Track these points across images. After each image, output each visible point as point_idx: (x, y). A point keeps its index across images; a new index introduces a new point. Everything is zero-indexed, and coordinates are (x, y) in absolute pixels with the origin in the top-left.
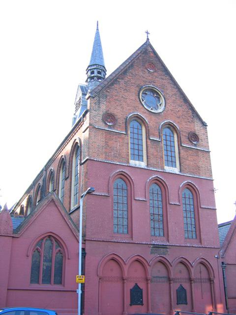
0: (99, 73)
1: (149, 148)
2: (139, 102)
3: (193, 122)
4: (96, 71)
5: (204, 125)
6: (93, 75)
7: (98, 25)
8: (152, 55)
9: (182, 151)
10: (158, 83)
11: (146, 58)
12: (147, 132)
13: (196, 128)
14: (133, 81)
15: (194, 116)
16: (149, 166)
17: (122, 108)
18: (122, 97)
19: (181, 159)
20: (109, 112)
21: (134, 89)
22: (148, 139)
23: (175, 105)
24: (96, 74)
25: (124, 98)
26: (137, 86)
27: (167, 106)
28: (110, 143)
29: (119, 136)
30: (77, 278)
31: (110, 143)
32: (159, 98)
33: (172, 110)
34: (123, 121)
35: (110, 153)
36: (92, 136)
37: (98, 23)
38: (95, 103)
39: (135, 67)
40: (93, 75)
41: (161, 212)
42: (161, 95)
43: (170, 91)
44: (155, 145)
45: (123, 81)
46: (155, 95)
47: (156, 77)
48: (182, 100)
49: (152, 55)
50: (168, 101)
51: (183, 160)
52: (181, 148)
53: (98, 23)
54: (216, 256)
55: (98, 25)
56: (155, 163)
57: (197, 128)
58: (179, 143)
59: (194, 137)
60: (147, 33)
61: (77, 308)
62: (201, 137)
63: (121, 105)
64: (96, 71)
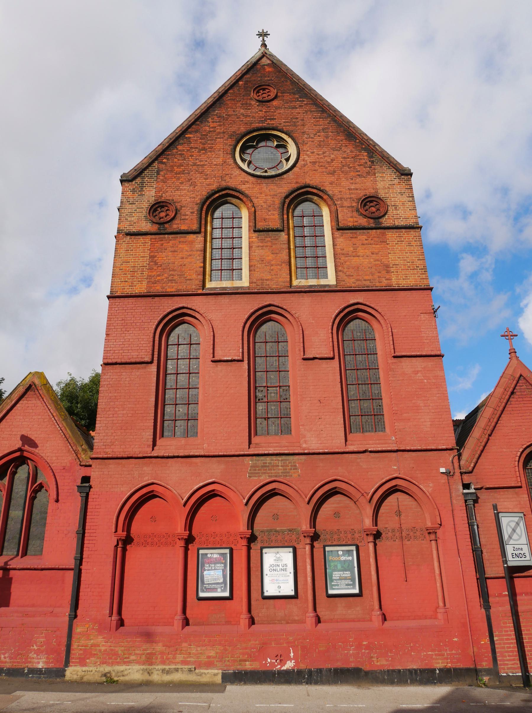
11: (264, 98)
13: (380, 185)
15: (373, 162)
16: (368, 336)
18: (195, 164)
23: (325, 149)
26: (231, 136)
29: (182, 239)
31: (164, 257)
32: (285, 147)
33: (314, 163)
35: (159, 276)
36: (122, 251)
38: (133, 191)
39: (228, 102)
41: (261, 407)
45: (198, 135)
46: (276, 143)
48: (341, 137)
52: (72, 672)
54: (443, 470)
56: (269, 277)
57: (383, 183)
59: (372, 207)
61: (335, 256)
63: (189, 180)
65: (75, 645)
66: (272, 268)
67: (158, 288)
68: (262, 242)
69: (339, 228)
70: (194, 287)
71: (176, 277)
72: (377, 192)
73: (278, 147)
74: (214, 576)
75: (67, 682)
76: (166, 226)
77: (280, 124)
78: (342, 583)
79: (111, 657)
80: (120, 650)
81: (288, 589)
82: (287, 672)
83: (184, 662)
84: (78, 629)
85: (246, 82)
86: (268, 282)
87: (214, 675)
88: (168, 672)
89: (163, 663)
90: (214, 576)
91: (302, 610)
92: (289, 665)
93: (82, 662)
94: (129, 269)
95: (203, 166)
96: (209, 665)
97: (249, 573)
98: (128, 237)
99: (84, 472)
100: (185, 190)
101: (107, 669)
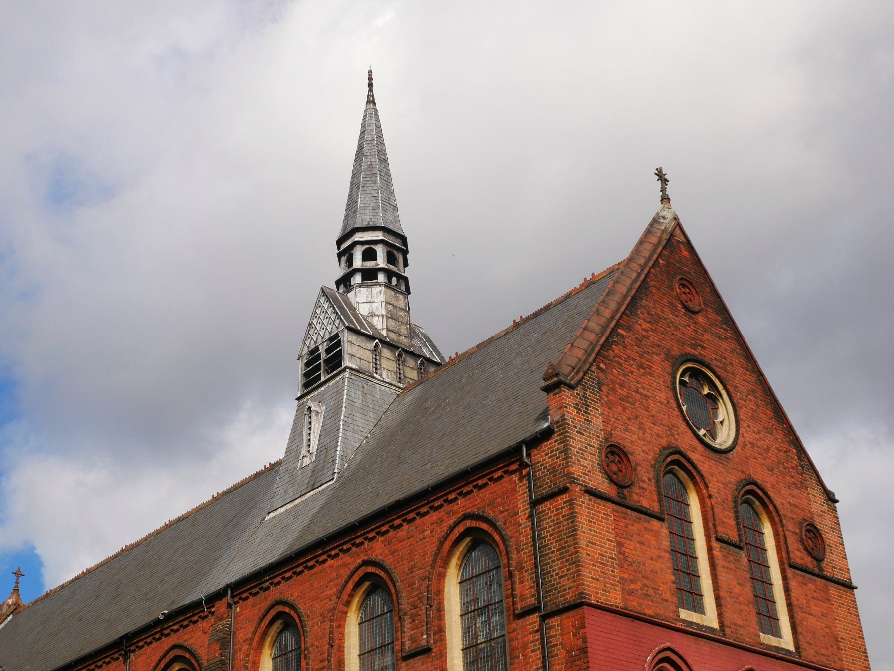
0: (391, 259)
1: (719, 569)
2: (677, 412)
3: (803, 486)
4: (381, 250)
5: (831, 499)
6: (370, 264)
7: (370, 86)
9: (793, 584)
10: (714, 348)
12: (710, 516)
14: (654, 338)
15: (802, 467)
18: (637, 391)
19: (795, 609)
20: (614, 440)
21: (659, 366)
22: (716, 545)
25: (641, 394)
27: (742, 430)
28: (631, 546)
29: (646, 524)
33: (753, 444)
34: (648, 473)
35: (632, 582)
37: (370, 79)
40: (370, 264)
42: (724, 393)
43: (741, 380)
44: (731, 558)
46: (706, 391)
47: (705, 330)
49: (686, 253)
50: (741, 414)
51: (799, 616)
52: (790, 572)
53: (370, 79)
55: (370, 86)
58: (784, 555)
64: (381, 250)
66: (742, 607)
67: (634, 605)
68: (726, 561)
69: (786, 564)
70: (672, 615)
71: (651, 592)
72: (812, 518)
73: (708, 395)
76: (625, 491)
77: (712, 360)
85: (668, 264)
86: (741, 631)
94: (597, 558)
95: (647, 397)
98: (587, 497)
100: (634, 433)
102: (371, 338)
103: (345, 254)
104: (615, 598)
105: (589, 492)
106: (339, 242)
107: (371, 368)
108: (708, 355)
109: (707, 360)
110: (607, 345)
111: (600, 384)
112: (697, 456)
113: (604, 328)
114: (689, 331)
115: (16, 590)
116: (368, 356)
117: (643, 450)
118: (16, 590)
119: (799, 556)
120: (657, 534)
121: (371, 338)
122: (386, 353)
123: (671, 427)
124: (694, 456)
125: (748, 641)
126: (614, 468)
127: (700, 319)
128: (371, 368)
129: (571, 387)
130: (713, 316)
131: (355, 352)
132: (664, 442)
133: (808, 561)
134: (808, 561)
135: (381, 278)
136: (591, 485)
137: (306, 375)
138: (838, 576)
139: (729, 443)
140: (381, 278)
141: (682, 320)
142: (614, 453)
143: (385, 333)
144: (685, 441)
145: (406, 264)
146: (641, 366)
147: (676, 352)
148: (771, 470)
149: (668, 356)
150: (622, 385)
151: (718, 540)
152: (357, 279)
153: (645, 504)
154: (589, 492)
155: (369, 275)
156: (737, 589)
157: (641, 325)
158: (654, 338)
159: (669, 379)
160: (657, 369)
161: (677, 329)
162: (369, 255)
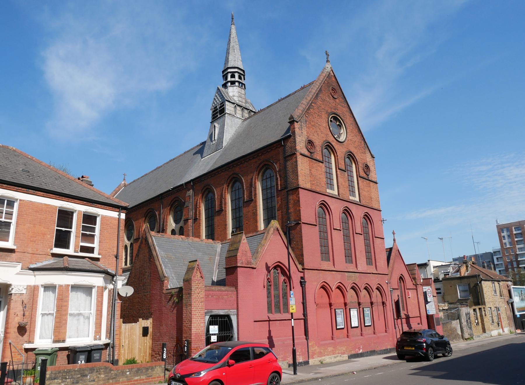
0: (240, 78)
1: (339, 178)
3: (365, 153)
4: (237, 75)
6: (233, 79)
8: (334, 79)
9: (360, 182)
10: (341, 111)
17: (318, 134)
21: (324, 116)
22: (338, 170)
24: (237, 79)
30: (291, 308)
46: (338, 123)
50: (348, 131)
51: (361, 191)
52: (359, 178)
60: (394, 233)
62: (372, 168)
64: (237, 75)
65: (310, 351)
67: (314, 188)
69: (359, 176)
74: (340, 319)
75: (312, 366)
78: (355, 322)
79: (320, 354)
80: (322, 351)
81: (357, 325)
82: (361, 354)
83: (339, 353)
84: (310, 344)
87: (345, 357)
88: (335, 357)
89: (333, 354)
90: (340, 319)
91: (358, 330)
92: (361, 351)
93: (313, 358)
96: (344, 353)
97: (348, 318)
99: (302, 275)
101: (320, 359)
102: (234, 103)
103: (225, 77)
104: (308, 186)
105: (301, 154)
106: (223, 72)
107: (233, 113)
108: (339, 112)
109: (338, 114)
110: (309, 109)
111: (306, 121)
112: (334, 143)
113: (308, 104)
114: (334, 105)
115: (124, 179)
116: (233, 109)
117: (318, 142)
118: (124, 179)
119: (362, 174)
120: (321, 167)
121: (234, 103)
122: (238, 108)
123: (327, 135)
124: (333, 144)
125: (346, 199)
126: (309, 147)
127: (337, 100)
128: (233, 113)
129: (297, 122)
130: (341, 99)
131: (229, 108)
132: (324, 139)
133: (364, 175)
134: (364, 175)
135: (237, 84)
136: (302, 152)
137: (213, 115)
138: (373, 180)
139: (344, 140)
140: (237, 84)
141: (332, 101)
142: (310, 142)
143: (238, 102)
144: (331, 139)
145: (244, 79)
146: (318, 115)
147: (329, 111)
148: (356, 148)
149: (327, 112)
150: (313, 122)
151: (339, 169)
152: (229, 84)
153: (318, 158)
154: (301, 154)
155: (233, 83)
156: (344, 184)
157: (319, 102)
158: (323, 107)
159: (327, 120)
160: (323, 116)
161: (330, 104)
162: (233, 76)
